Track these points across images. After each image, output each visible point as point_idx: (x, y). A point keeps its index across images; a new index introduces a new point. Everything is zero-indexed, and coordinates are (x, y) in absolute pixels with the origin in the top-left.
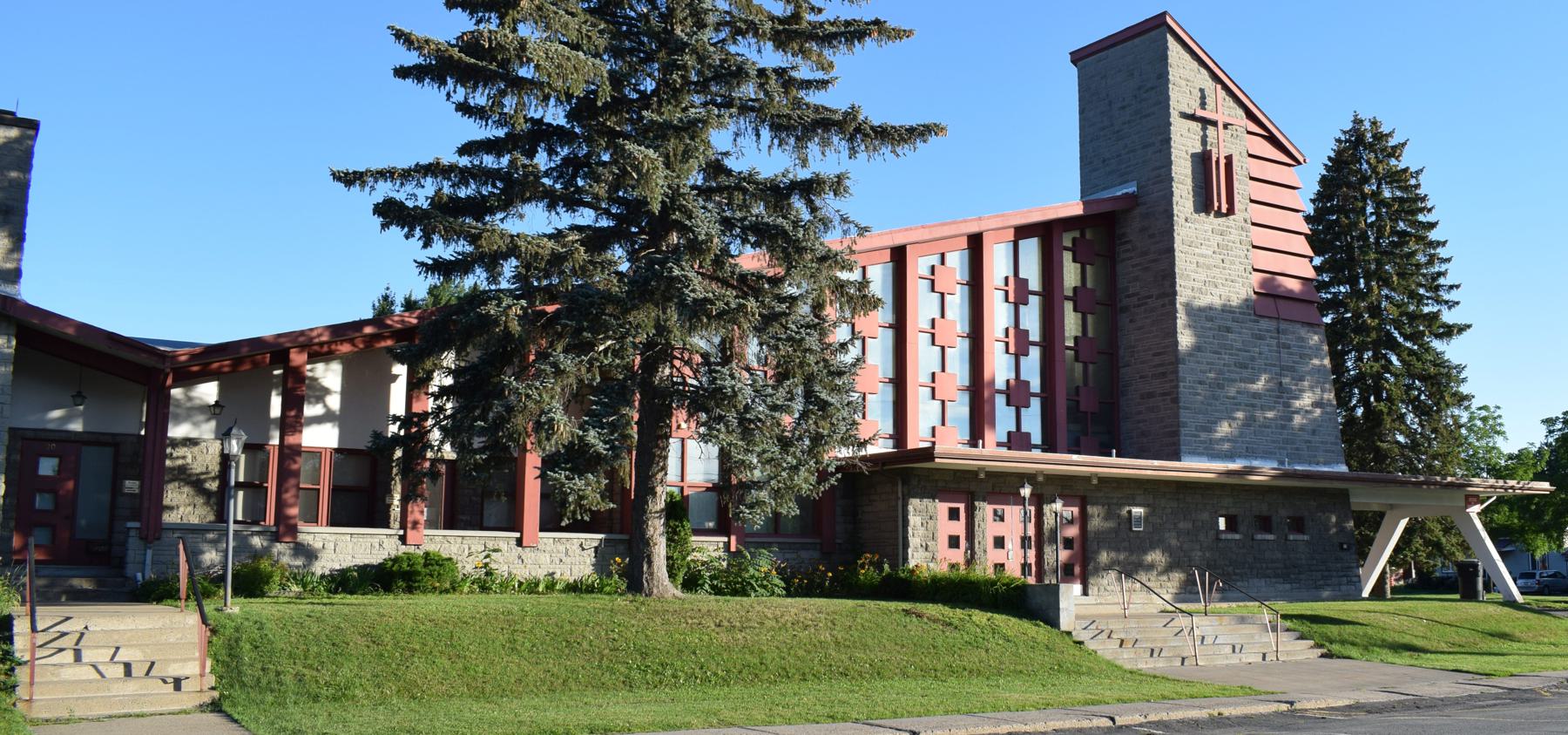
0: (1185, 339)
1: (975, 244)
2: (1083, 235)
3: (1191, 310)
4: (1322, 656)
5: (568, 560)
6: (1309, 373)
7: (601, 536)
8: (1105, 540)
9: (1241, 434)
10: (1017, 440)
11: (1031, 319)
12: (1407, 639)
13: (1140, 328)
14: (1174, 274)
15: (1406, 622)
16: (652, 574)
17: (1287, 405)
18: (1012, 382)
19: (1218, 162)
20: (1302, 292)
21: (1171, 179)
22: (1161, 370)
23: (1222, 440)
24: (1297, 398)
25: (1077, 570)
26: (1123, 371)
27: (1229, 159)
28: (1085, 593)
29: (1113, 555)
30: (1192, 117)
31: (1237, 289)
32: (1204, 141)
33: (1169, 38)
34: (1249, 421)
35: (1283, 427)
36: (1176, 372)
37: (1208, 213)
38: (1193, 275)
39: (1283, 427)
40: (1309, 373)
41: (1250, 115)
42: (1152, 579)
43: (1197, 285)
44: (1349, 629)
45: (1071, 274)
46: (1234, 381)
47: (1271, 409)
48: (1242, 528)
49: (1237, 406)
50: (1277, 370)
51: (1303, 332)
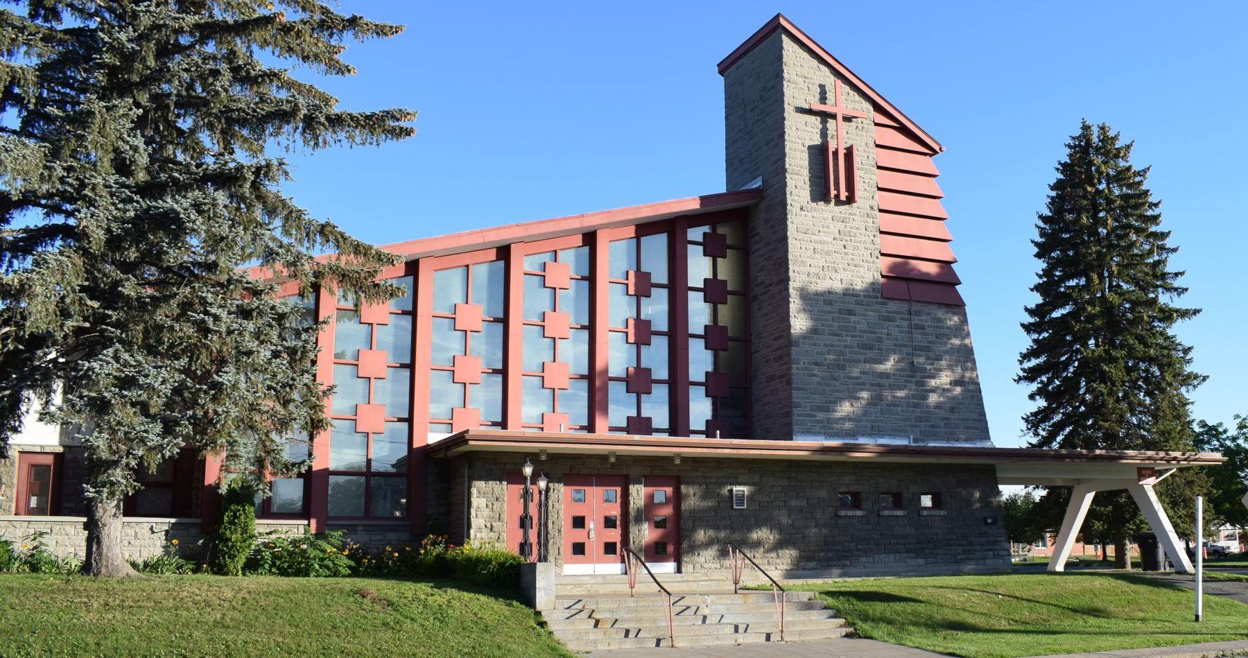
0: (799, 323)
1: (590, 239)
2: (714, 229)
3: (805, 296)
4: (848, 636)
5: (137, 543)
6: (946, 352)
7: (173, 520)
8: (700, 519)
9: (865, 414)
10: (639, 424)
11: (657, 309)
12: (951, 616)
13: (765, 315)
14: (787, 260)
15: (975, 597)
16: (100, 554)
17: (923, 384)
18: (631, 370)
19: (836, 153)
20: (939, 275)
21: (785, 171)
22: (779, 353)
23: (843, 419)
24: (933, 377)
25: (670, 548)
26: (754, 356)
27: (849, 153)
28: (679, 571)
29: (711, 533)
30: (810, 112)
31: (863, 271)
32: (824, 133)
33: (784, 36)
34: (875, 401)
35: (916, 406)
36: (789, 355)
37: (827, 201)
38: (812, 262)
39: (916, 406)
40: (946, 352)
41: (878, 108)
42: (759, 556)
43: (813, 270)
44: (898, 606)
45: (699, 268)
46: (858, 361)
47: (900, 388)
48: (865, 505)
49: (862, 386)
50: (909, 350)
51: (940, 313)
